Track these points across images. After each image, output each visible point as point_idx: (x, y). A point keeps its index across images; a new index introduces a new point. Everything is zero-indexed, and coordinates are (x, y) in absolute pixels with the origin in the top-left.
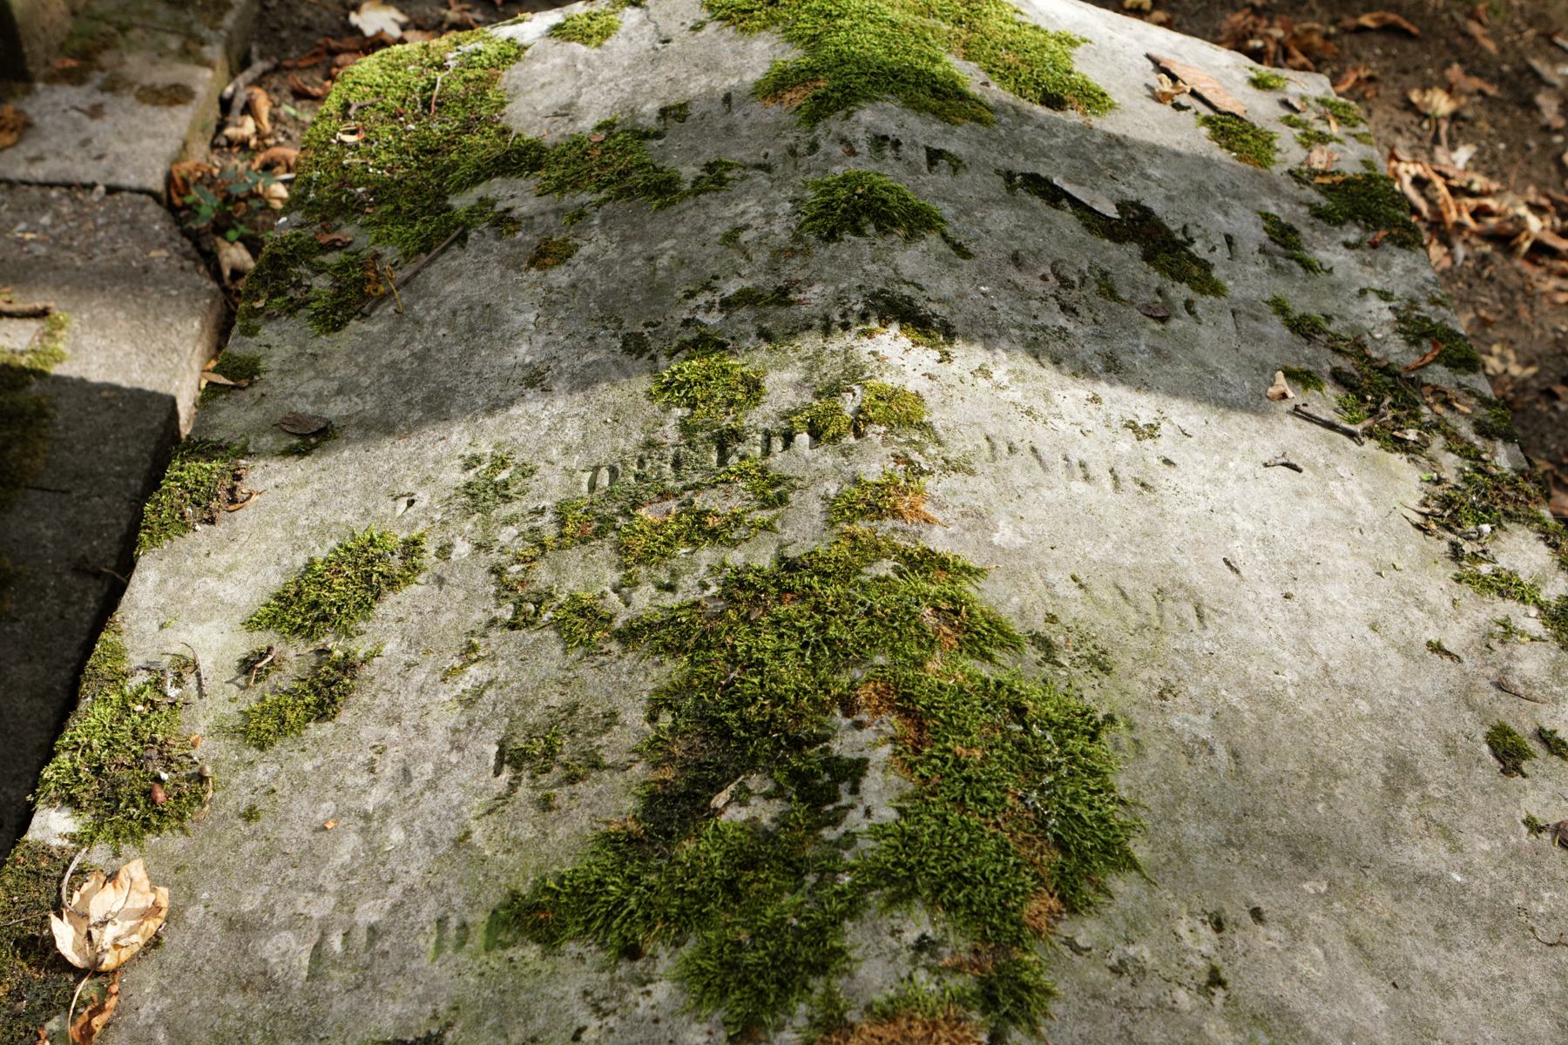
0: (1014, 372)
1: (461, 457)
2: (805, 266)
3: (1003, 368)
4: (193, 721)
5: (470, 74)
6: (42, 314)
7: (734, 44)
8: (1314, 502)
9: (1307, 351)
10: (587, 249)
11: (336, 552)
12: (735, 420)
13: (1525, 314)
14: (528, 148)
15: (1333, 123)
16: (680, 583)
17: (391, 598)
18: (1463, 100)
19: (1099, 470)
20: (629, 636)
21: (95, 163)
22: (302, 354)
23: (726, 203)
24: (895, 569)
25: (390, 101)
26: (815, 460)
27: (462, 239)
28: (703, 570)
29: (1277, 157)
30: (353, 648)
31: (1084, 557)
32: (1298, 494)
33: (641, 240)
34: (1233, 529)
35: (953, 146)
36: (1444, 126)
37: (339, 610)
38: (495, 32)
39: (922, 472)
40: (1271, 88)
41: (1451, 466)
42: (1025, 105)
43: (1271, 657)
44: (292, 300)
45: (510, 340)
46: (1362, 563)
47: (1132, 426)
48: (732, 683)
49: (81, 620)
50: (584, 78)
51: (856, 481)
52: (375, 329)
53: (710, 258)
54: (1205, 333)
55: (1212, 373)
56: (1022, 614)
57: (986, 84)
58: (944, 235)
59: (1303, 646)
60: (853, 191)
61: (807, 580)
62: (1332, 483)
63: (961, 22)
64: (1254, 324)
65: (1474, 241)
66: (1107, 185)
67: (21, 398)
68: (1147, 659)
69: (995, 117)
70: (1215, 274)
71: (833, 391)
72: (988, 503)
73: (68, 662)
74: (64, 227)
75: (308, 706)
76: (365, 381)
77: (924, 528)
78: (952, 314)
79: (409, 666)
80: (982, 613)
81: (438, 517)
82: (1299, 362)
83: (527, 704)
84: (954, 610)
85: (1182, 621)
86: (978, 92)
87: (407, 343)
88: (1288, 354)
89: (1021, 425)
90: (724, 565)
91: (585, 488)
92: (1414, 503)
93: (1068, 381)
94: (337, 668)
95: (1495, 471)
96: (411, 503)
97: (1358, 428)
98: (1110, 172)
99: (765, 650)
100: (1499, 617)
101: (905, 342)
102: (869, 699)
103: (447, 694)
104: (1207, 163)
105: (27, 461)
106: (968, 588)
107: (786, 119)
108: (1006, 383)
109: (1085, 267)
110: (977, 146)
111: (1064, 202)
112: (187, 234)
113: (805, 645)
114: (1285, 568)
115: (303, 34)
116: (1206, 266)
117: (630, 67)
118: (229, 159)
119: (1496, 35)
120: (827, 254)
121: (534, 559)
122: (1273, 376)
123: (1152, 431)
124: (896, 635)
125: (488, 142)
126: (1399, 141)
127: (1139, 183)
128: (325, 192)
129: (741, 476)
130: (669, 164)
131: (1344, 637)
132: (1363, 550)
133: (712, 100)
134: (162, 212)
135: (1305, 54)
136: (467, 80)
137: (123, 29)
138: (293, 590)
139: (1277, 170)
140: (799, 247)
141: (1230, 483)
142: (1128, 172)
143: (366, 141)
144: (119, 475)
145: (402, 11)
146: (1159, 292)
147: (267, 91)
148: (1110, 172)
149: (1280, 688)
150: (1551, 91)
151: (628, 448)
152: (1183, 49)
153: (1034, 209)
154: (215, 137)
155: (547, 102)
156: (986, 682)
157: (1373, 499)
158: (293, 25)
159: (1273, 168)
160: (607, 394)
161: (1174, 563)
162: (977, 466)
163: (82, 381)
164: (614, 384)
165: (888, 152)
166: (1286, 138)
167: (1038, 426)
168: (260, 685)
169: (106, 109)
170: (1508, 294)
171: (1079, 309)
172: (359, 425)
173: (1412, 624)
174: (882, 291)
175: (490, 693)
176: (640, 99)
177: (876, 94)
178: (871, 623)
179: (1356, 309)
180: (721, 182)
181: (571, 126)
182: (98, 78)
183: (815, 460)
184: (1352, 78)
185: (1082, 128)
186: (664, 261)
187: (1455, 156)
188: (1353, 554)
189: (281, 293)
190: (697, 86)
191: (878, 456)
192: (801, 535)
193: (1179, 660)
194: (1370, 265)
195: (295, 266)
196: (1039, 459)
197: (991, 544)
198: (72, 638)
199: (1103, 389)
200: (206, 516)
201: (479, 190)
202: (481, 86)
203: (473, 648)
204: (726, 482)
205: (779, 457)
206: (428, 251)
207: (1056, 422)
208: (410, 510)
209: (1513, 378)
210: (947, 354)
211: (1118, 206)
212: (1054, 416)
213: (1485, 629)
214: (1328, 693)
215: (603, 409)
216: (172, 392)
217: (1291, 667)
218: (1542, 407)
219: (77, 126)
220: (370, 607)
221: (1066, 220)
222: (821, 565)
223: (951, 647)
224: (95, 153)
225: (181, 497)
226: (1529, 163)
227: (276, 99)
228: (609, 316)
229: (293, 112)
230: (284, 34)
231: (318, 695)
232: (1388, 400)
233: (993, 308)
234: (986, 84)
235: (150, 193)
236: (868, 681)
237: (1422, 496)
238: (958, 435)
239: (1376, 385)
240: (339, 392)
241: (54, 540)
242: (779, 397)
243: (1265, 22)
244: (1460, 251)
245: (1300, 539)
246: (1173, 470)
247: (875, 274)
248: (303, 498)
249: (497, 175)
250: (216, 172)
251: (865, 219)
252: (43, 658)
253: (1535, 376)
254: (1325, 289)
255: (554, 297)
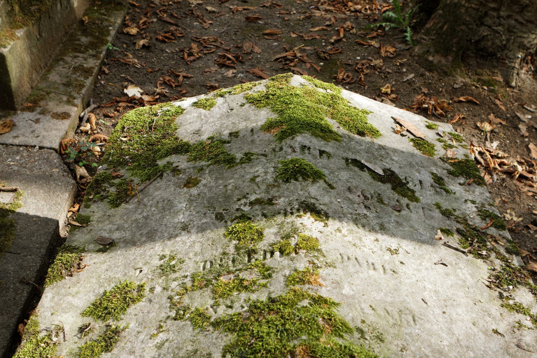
0: (349, 230)
1: (159, 255)
2: (278, 191)
3: (346, 229)
4: (61, 351)
5: (165, 118)
6: (15, 191)
7: (254, 112)
8: (452, 277)
9: (448, 222)
10: (204, 182)
11: (114, 288)
12: (254, 246)
13: (518, 199)
14: (184, 145)
15: (454, 141)
16: (234, 305)
17: (133, 307)
18: (495, 126)
19: (379, 266)
20: (216, 324)
21: (36, 139)
22: (105, 215)
23: (251, 168)
24: (309, 303)
25: (138, 127)
26: (281, 262)
27: (161, 176)
28: (242, 301)
29: (436, 153)
30: (119, 325)
31: (374, 298)
32: (446, 274)
33: (222, 179)
34: (425, 288)
35: (328, 149)
36: (489, 135)
37: (114, 310)
38: (174, 103)
39: (318, 267)
40: (433, 129)
41: (498, 264)
42: (352, 135)
43: (439, 336)
44: (102, 196)
45: (177, 213)
46: (469, 300)
47: (389, 250)
48: (252, 344)
49: (21, 300)
50: (204, 121)
51: (296, 270)
52: (130, 207)
53: (246, 187)
54: (413, 216)
55: (416, 230)
56: (353, 320)
57: (339, 127)
58: (325, 181)
59: (450, 332)
60: (295, 165)
61: (278, 306)
62: (458, 270)
63: (330, 106)
64: (430, 212)
65: (500, 174)
66: (379, 163)
67: (6, 220)
68: (396, 336)
69: (342, 139)
70: (416, 194)
71: (287, 237)
72: (341, 278)
73: (15, 315)
74: (24, 160)
75: (102, 346)
76: (126, 226)
77: (319, 287)
78: (328, 209)
79: (138, 332)
80: (339, 320)
81: (150, 277)
82: (445, 227)
83: (180, 349)
84: (329, 319)
85: (408, 322)
86: (336, 130)
87: (141, 213)
88: (441, 223)
89: (352, 250)
90: (250, 299)
91: (201, 268)
92: (486, 277)
93: (367, 233)
94: (113, 332)
95: (513, 266)
96: (141, 271)
97: (466, 250)
98: (380, 158)
99: (264, 332)
100: (517, 320)
101: (312, 219)
102: (300, 352)
103: (152, 344)
104: (413, 155)
105: (6, 243)
106: (334, 310)
107: (272, 139)
108: (346, 234)
109: (372, 192)
110: (336, 149)
111: (365, 169)
112: (65, 163)
113: (278, 331)
114: (443, 302)
115: (108, 96)
116: (413, 192)
117: (219, 118)
118: (81, 137)
119: (505, 104)
120: (286, 187)
121: (183, 294)
122: (437, 231)
123: (396, 252)
124: (309, 328)
125: (171, 142)
126: (474, 139)
127: (390, 162)
128: (115, 157)
129: (256, 267)
130: (232, 153)
131: (464, 328)
132: (469, 295)
133: (247, 131)
134: (57, 155)
135: (442, 110)
136: (164, 120)
137: (48, 93)
138: (99, 302)
139: (436, 157)
140: (276, 184)
141: (423, 271)
142: (386, 158)
143: (130, 140)
144: (37, 248)
145: (141, 89)
146: (398, 201)
147: (95, 114)
148: (380, 158)
149: (442, 347)
150: (523, 123)
151: (217, 254)
152: (404, 115)
153: (355, 171)
154: (77, 130)
155: (191, 129)
156: (341, 346)
157: (472, 276)
158: (105, 92)
159: (434, 156)
160: (210, 234)
161: (405, 301)
162: (337, 265)
163: (27, 214)
164: (212, 231)
165: (306, 151)
166: (439, 146)
167: (357, 250)
168: (86, 337)
169: (41, 120)
170: (512, 193)
171: (371, 207)
172: (124, 242)
173: (487, 323)
174: (304, 201)
175: (167, 344)
176: (223, 129)
177: (302, 131)
178: (301, 324)
179: (464, 207)
180: (250, 160)
181: (199, 138)
182: (38, 110)
183: (281, 262)
184: (458, 118)
185: (371, 143)
186: (230, 187)
187: (492, 145)
188: (466, 297)
189: (99, 193)
190: (242, 126)
191: (303, 261)
192: (277, 289)
193: (407, 337)
194: (468, 191)
195: (104, 184)
196: (358, 262)
197: (342, 294)
198: (17, 307)
199: (379, 236)
200: (69, 274)
201: (167, 159)
202: (169, 123)
203: (161, 327)
204: (251, 268)
205: (269, 260)
206: (149, 180)
207: (364, 248)
208: (141, 274)
209: (514, 222)
210: (326, 224)
211: (383, 170)
212: (363, 246)
213: (512, 325)
214: (459, 349)
215: (208, 240)
216: (58, 219)
217: (446, 339)
218: (525, 232)
219: (31, 126)
220: (125, 310)
221: (366, 175)
222: (283, 301)
223: (329, 333)
224: (36, 135)
225: (61, 266)
226: (517, 147)
227: (98, 117)
228: (211, 206)
229: (103, 122)
230: (102, 96)
231: (106, 342)
232: (476, 240)
233: (342, 207)
234: (339, 127)
235: (54, 149)
236: (300, 345)
237: (489, 275)
238: (330, 254)
239: (472, 234)
240: (117, 229)
241: (14, 271)
242: (269, 238)
243: (428, 99)
244: (495, 177)
245: (448, 291)
246: (404, 266)
247: (302, 195)
248: (103, 268)
249: (174, 154)
250: (76, 142)
251: (298, 175)
252: (7, 314)
253: (522, 221)
254: (453, 199)
255: (192, 198)
